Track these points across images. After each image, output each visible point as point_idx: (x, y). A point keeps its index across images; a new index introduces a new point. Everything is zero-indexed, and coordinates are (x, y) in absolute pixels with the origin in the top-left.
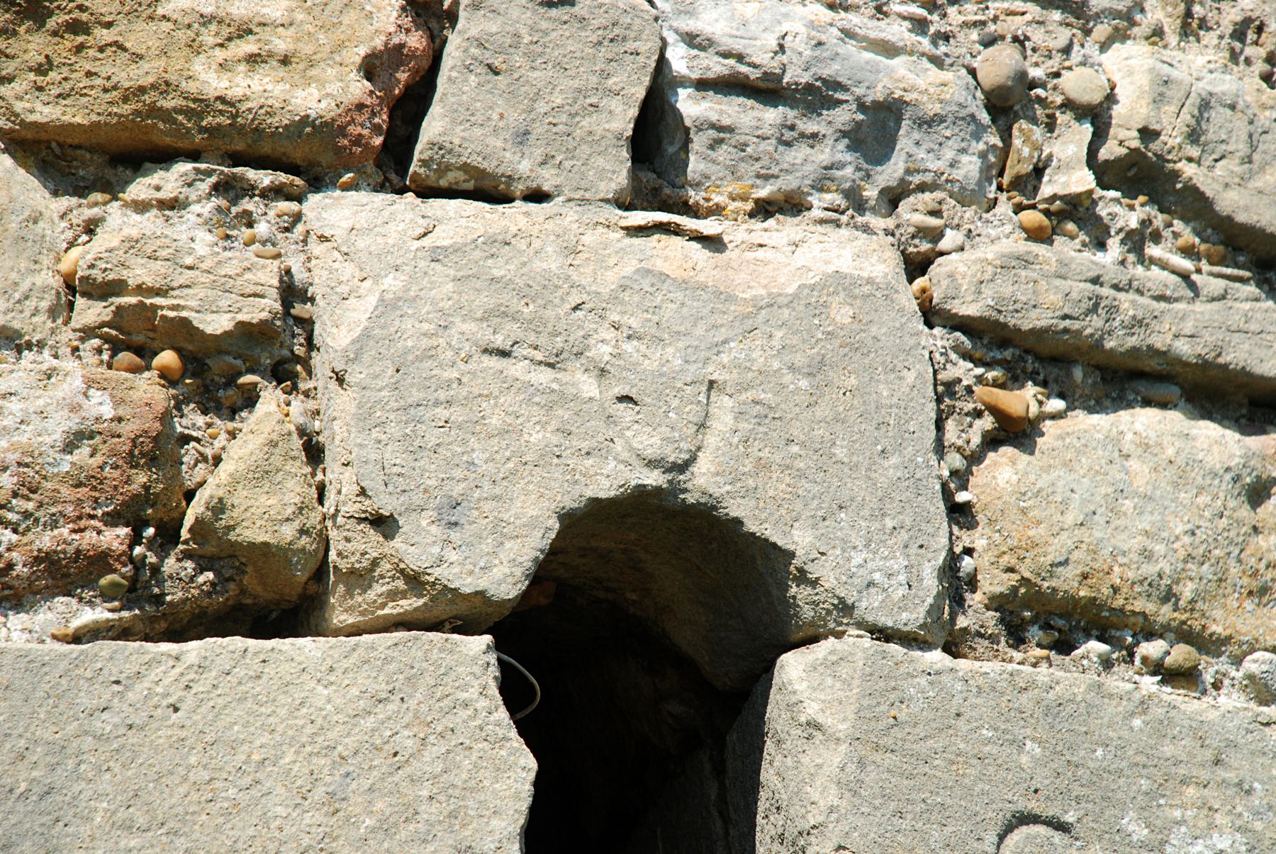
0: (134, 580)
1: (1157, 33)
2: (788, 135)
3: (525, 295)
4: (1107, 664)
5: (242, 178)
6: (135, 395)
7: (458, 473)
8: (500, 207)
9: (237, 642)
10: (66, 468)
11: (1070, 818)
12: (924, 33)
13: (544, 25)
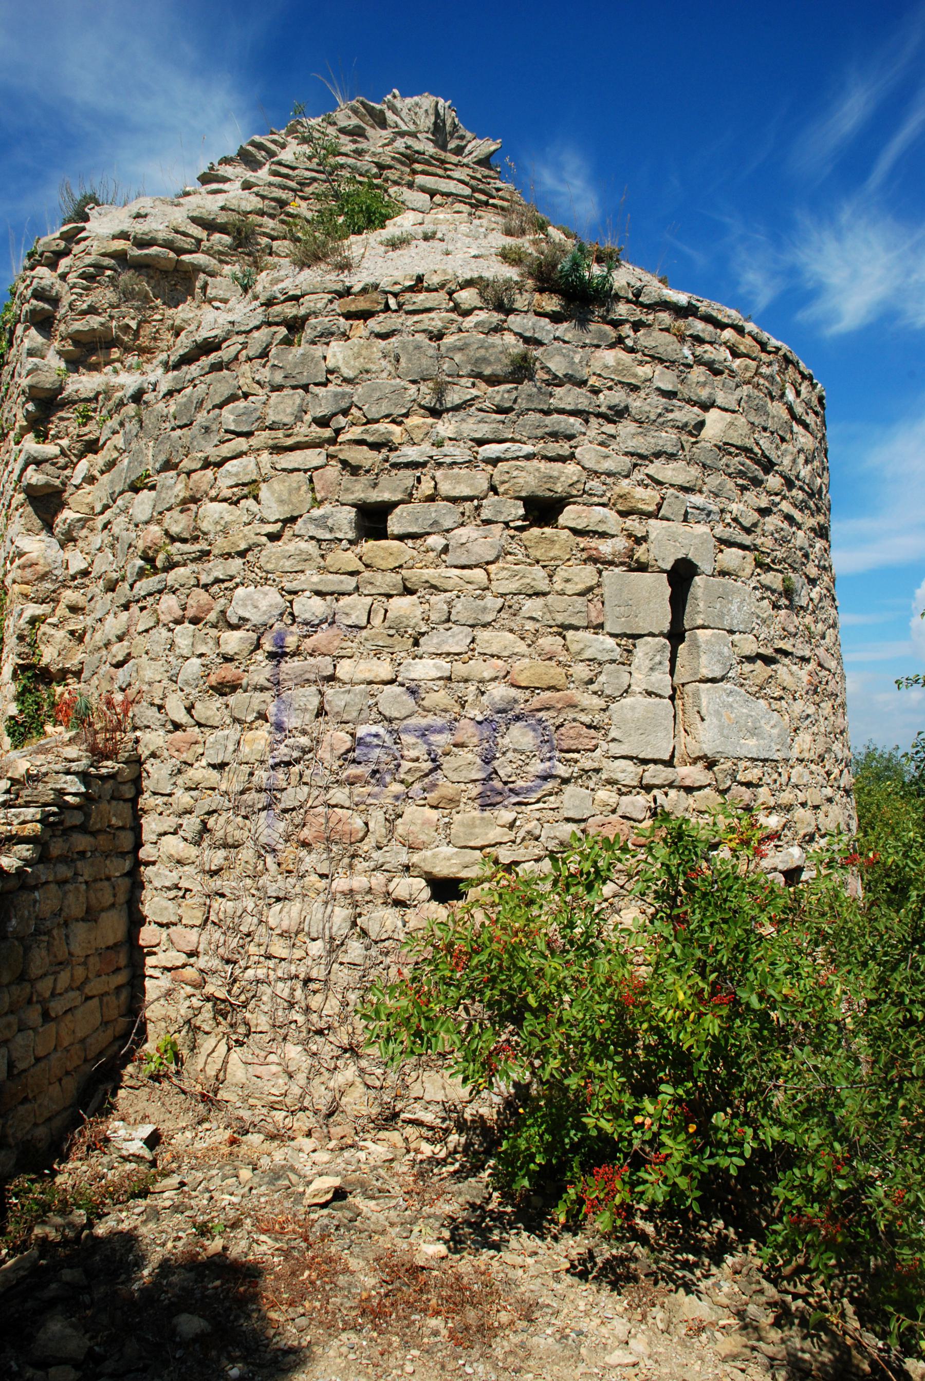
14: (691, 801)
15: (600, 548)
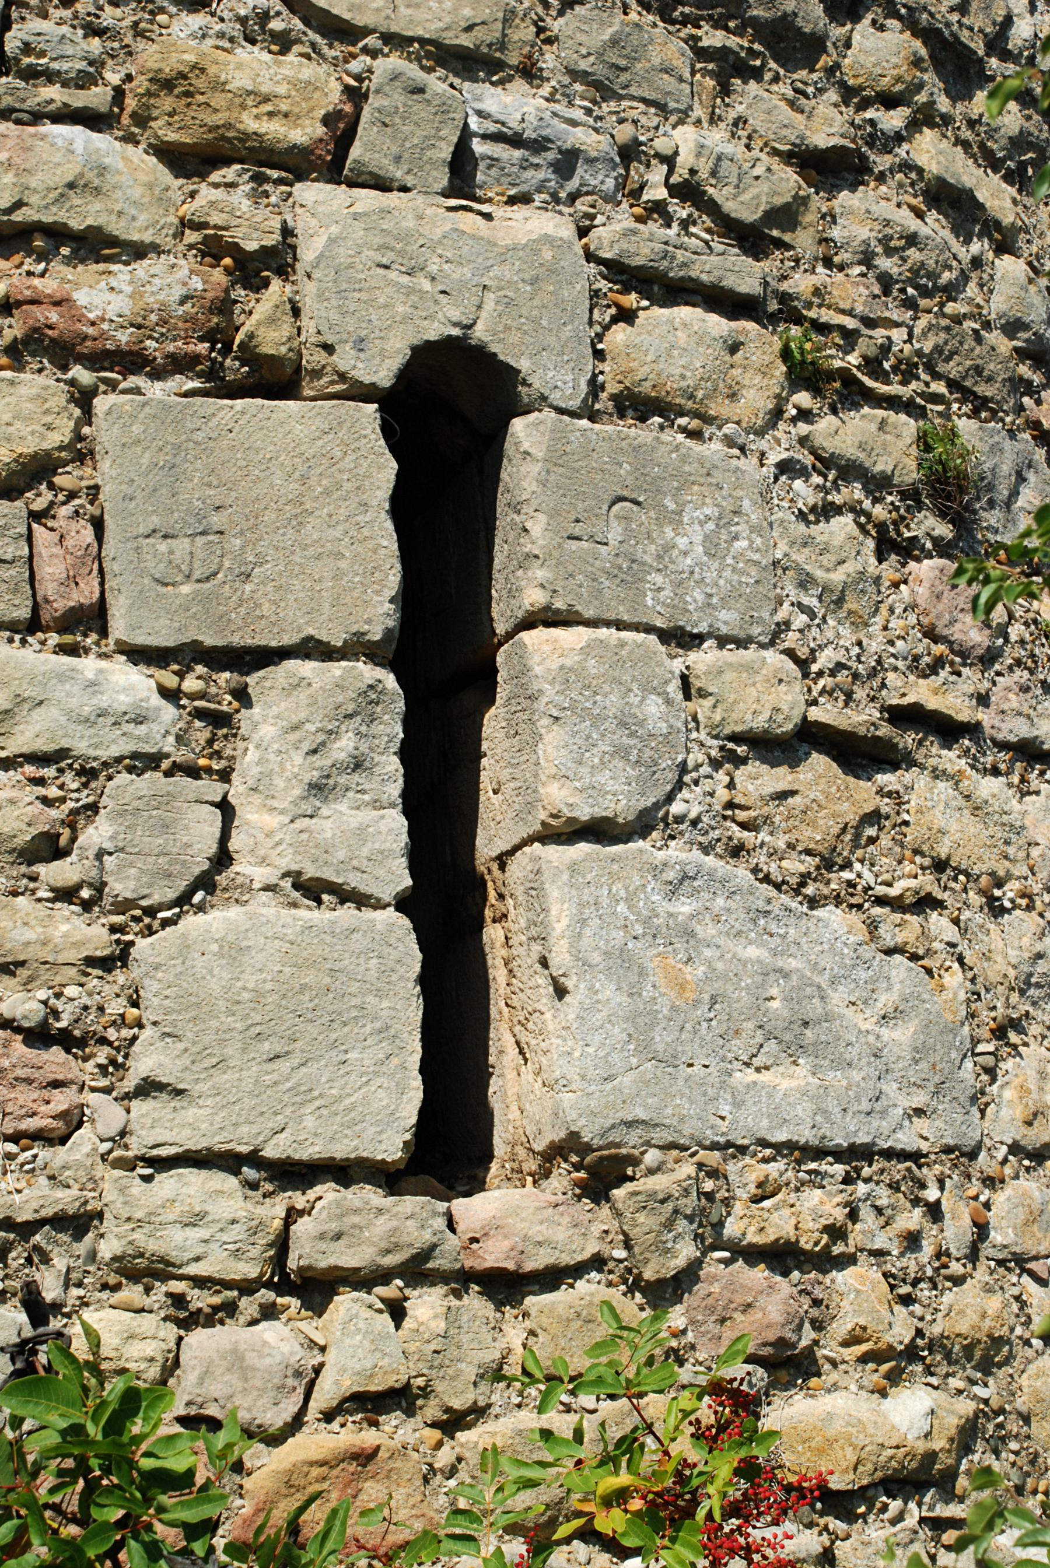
0: (211, 368)
1: (698, 122)
2: (525, 164)
3: (398, 238)
4: (662, 427)
5: (264, 174)
6: (213, 279)
7: (364, 325)
8: (387, 194)
9: (259, 401)
10: (180, 313)
11: (641, 499)
12: (590, 116)
13: (410, 103)
14: (514, 1335)
15: (81, 297)
